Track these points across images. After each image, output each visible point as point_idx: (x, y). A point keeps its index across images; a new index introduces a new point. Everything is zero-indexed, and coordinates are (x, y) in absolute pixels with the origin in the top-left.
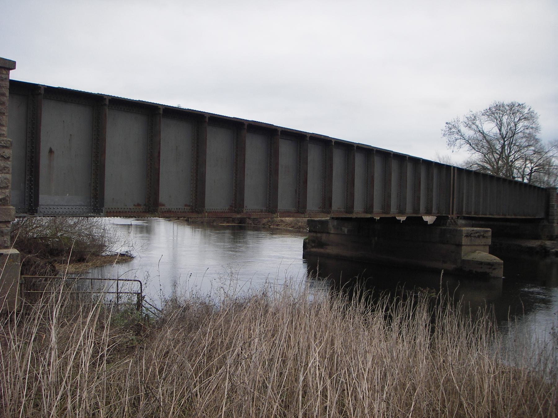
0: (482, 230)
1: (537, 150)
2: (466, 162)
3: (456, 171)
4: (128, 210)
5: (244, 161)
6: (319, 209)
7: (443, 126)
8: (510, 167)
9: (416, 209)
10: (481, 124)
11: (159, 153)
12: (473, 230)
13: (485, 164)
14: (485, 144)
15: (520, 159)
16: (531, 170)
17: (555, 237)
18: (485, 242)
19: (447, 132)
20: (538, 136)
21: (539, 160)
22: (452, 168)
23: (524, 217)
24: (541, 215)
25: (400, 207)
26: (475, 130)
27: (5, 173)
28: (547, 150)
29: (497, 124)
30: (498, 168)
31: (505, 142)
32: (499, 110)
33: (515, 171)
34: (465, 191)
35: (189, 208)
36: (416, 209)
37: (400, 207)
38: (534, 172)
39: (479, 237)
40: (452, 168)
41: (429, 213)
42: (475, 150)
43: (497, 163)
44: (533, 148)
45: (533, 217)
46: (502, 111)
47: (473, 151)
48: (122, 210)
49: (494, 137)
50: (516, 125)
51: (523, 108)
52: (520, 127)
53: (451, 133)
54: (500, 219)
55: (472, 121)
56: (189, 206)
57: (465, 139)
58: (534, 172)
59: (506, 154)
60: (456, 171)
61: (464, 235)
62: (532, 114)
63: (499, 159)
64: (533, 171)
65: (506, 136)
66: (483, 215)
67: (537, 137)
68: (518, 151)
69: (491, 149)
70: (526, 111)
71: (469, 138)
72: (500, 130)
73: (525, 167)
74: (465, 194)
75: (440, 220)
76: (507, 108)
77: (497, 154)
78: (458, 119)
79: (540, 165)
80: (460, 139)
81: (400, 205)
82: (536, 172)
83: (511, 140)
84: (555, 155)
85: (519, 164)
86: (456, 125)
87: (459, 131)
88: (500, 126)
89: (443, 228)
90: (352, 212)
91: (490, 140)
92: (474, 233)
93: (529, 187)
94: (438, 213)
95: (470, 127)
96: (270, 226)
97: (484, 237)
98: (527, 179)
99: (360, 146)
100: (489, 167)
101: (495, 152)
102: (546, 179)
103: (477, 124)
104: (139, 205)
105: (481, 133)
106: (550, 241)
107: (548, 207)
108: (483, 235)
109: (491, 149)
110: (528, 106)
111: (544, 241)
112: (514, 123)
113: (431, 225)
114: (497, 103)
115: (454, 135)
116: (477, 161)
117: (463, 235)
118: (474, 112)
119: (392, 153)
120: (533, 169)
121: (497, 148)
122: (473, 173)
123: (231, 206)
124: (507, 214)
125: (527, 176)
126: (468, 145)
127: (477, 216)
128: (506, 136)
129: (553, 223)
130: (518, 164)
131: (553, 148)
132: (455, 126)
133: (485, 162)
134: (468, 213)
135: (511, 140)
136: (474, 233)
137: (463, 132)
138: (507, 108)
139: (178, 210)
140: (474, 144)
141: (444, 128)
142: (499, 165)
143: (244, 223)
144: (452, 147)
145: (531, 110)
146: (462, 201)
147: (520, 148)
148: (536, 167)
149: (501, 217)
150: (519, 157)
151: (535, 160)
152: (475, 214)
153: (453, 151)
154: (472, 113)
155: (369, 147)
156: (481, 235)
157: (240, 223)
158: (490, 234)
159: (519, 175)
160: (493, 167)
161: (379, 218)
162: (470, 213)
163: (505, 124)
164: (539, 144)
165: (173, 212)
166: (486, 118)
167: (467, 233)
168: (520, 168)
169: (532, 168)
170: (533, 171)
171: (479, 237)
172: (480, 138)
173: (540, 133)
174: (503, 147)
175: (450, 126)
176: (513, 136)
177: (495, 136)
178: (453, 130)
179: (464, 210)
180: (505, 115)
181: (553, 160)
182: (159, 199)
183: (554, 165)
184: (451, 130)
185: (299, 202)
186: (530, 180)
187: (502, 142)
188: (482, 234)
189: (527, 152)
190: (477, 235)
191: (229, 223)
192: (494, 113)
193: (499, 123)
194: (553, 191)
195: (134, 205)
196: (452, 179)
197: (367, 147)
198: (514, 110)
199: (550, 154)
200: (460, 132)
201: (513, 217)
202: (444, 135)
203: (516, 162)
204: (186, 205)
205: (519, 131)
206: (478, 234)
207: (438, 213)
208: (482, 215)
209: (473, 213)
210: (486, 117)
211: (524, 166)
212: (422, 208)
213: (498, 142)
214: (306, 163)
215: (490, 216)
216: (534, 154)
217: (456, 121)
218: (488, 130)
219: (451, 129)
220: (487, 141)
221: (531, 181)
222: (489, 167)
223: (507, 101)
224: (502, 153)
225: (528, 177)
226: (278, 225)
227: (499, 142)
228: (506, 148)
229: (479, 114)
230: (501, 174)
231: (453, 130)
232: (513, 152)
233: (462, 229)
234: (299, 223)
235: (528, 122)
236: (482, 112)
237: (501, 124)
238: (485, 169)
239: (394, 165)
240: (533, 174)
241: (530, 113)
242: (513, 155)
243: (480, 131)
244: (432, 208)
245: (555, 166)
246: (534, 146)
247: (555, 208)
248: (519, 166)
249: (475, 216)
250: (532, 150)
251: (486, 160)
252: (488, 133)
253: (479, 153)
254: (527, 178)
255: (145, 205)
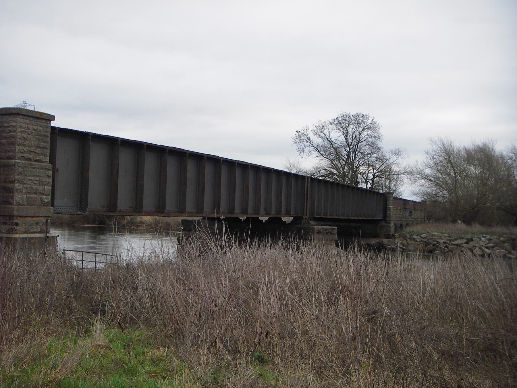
0: (330, 228)
1: (379, 157)
2: (314, 167)
3: (309, 180)
4: (98, 210)
5: (166, 176)
6: (211, 211)
7: (294, 134)
8: (355, 172)
9: (279, 212)
10: (329, 132)
11: (118, 171)
12: (323, 228)
13: (332, 169)
14: (333, 151)
15: (364, 165)
16: (374, 176)
17: (391, 235)
18: (332, 238)
19: (297, 140)
20: (380, 144)
21: (380, 166)
22: (306, 178)
23: (364, 218)
24: (380, 216)
25: (266, 209)
26: (323, 138)
27: (48, 186)
28: (388, 158)
29: (344, 133)
30: (344, 173)
31: (350, 149)
32: (346, 120)
33: (359, 176)
34: (316, 197)
35: (131, 209)
36: (279, 212)
37: (266, 209)
38: (377, 177)
39: (327, 233)
40: (306, 178)
41: (288, 214)
42: (323, 156)
43: (343, 169)
44: (375, 155)
45: (372, 218)
46: (348, 121)
47: (321, 157)
48: (94, 210)
49: (340, 145)
50: (360, 134)
51: (366, 119)
52: (364, 136)
53: (301, 141)
54: (345, 219)
55: (320, 130)
56: (131, 207)
57: (313, 146)
58: (377, 177)
59: (352, 160)
60: (309, 180)
61: (316, 232)
62: (375, 124)
63: (345, 165)
64: (376, 176)
65: (351, 144)
66: (331, 216)
67: (378, 146)
68: (362, 158)
69: (338, 155)
70: (369, 121)
71: (318, 145)
72: (346, 139)
73: (368, 172)
74: (316, 199)
75: (297, 220)
76: (353, 118)
77: (343, 160)
78: (307, 127)
79: (381, 171)
80: (309, 146)
81: (266, 208)
82: (378, 177)
83: (356, 148)
84: (395, 162)
85: (363, 170)
86: (306, 133)
87: (308, 139)
88: (346, 135)
89: (299, 226)
90: (233, 213)
91: (337, 148)
92: (324, 231)
93: (371, 193)
94: (295, 214)
95: (318, 135)
96: (130, 227)
97: (331, 233)
98: (370, 184)
99: (239, 162)
100: (335, 172)
101: (342, 158)
102: (387, 183)
103: (325, 133)
104: (103, 207)
105: (329, 140)
106: (387, 239)
107: (385, 209)
108: (331, 232)
109: (338, 155)
110: (371, 117)
111: (382, 239)
112: (359, 132)
113: (289, 224)
114: (344, 114)
115: (304, 142)
116: (325, 167)
117: (315, 232)
118: (323, 122)
119: (262, 167)
120: (376, 174)
121: (343, 154)
122: (323, 181)
123: (156, 208)
124: (351, 216)
125: (370, 181)
126: (317, 152)
127: (325, 217)
128: (351, 144)
129: (390, 223)
130: (362, 169)
131: (393, 156)
132: (304, 133)
133: (332, 168)
134: (318, 214)
135: (356, 148)
136: (324, 231)
137: (312, 140)
138: (353, 118)
139: (126, 210)
140: (321, 151)
141: (294, 136)
142: (345, 170)
143: (105, 224)
144: (302, 153)
145: (373, 121)
146: (314, 205)
147: (364, 155)
148: (378, 172)
149: (345, 218)
150: (363, 163)
151: (377, 166)
152: (324, 215)
153: (302, 158)
154: (321, 123)
155: (246, 163)
156: (329, 232)
157: (100, 224)
158: (336, 231)
159: (363, 180)
160: (339, 173)
161: (245, 218)
162: (320, 214)
163: (351, 134)
164: (381, 152)
165: (123, 212)
166: (333, 127)
167: (318, 230)
168: (364, 173)
169: (374, 174)
170: (376, 176)
171: (327, 233)
172: (328, 145)
173: (382, 142)
174: (349, 153)
175: (300, 134)
176: (358, 144)
177: (341, 143)
178: (303, 138)
179: (315, 211)
180: (351, 124)
181: (394, 166)
182: (117, 203)
183: (394, 171)
184: (301, 138)
185: (198, 205)
186: (372, 184)
187: (348, 149)
188: (330, 231)
189: (370, 159)
190: (326, 232)
191: (89, 224)
192: (341, 123)
193: (345, 132)
194: (390, 195)
195: (101, 207)
196: (306, 184)
197: (244, 163)
198: (359, 120)
199: (391, 161)
200: (309, 140)
201: (356, 218)
202: (295, 143)
203: (361, 168)
204: (130, 207)
205: (363, 140)
206: (327, 231)
207: (295, 214)
208: (329, 216)
209: (322, 214)
210: (333, 126)
211: (367, 172)
212: (283, 211)
213: (344, 149)
214: (204, 177)
215: (337, 217)
216: (376, 161)
217: (305, 129)
218: (335, 138)
219: (300, 137)
220: (334, 148)
221: (374, 185)
222: (335, 172)
223: (352, 112)
224: (347, 159)
225: (371, 182)
226: (138, 226)
227: (345, 149)
228: (351, 154)
229: (327, 123)
230: (347, 178)
231: (303, 138)
232: (358, 159)
233: (314, 227)
234: (159, 224)
235: (371, 131)
236: (330, 122)
237: (347, 133)
238: (332, 174)
239: (263, 176)
240: (375, 179)
241: (373, 123)
242: (357, 161)
243: (327, 139)
244: (290, 210)
245: (394, 172)
246: (377, 154)
247: (392, 210)
248: (363, 172)
249: (324, 217)
250: (375, 157)
251: (332, 166)
252: (335, 141)
253: (327, 159)
254: (370, 182)
255: (107, 207)
